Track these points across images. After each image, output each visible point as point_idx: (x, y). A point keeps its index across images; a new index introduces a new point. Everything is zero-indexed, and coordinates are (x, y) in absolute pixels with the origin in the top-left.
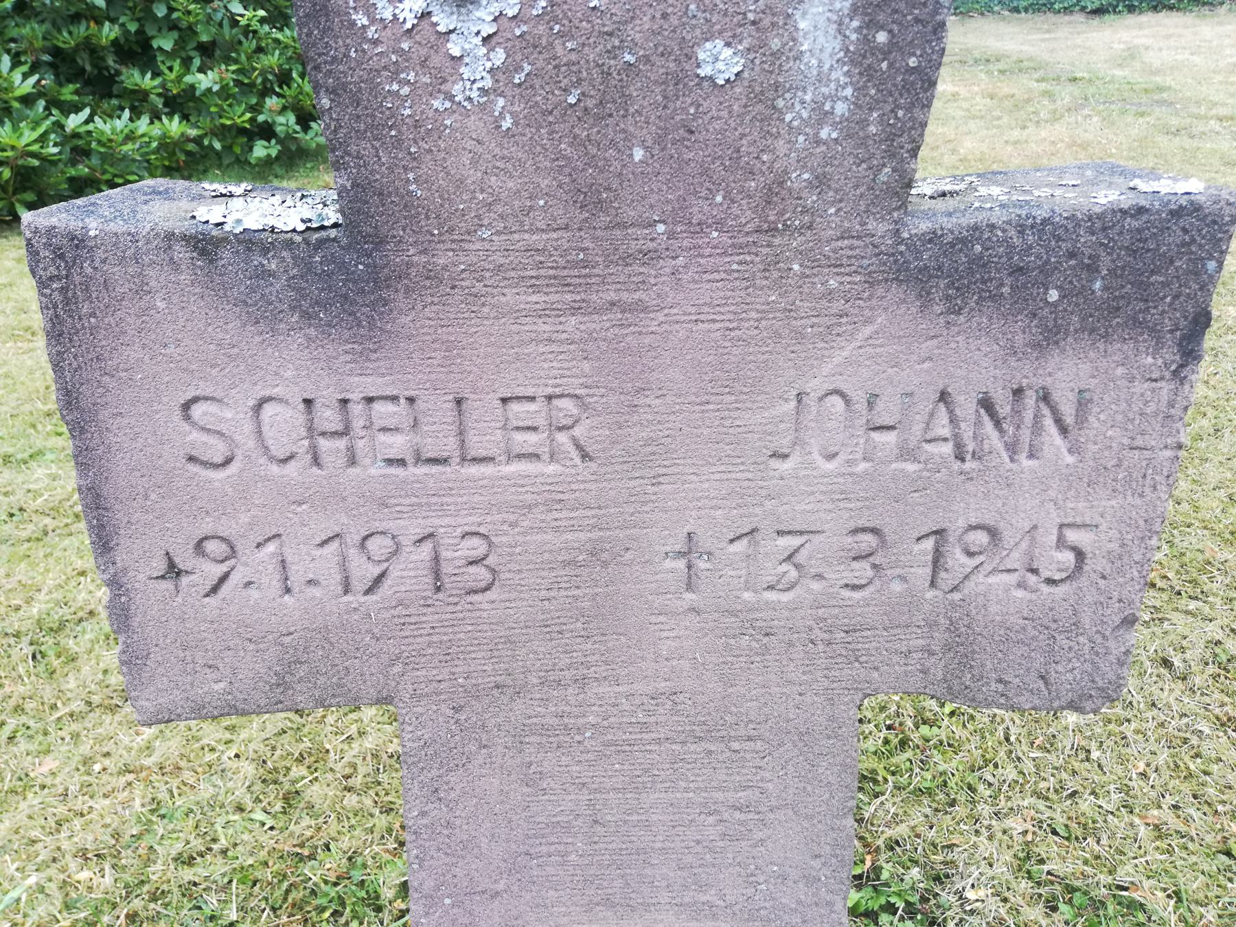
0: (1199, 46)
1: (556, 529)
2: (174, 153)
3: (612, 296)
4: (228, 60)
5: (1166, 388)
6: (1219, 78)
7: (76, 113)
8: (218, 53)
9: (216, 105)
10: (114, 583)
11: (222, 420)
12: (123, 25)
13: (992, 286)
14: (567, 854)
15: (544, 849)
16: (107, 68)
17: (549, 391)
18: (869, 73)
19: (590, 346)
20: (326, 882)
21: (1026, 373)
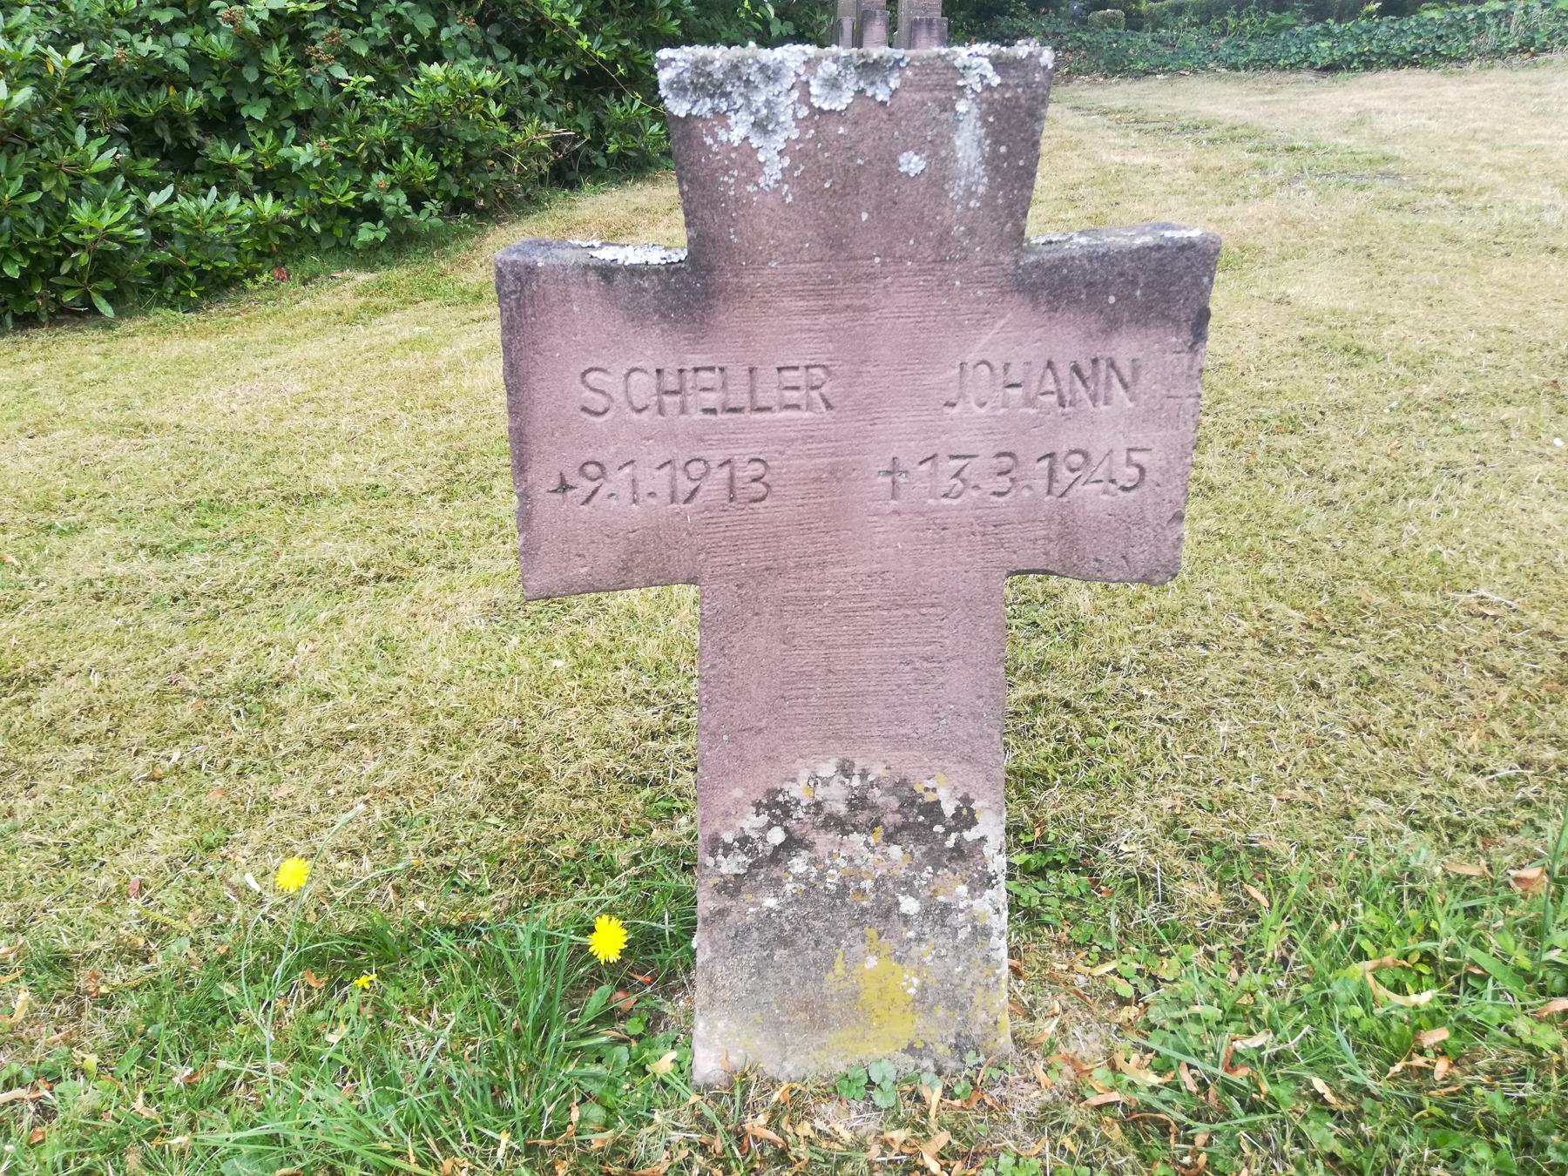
0: (1440, 110)
1: (809, 456)
2: (267, 237)
3: (847, 302)
4: (327, 131)
5: (1186, 358)
6: (1457, 146)
7: (158, 191)
8: (315, 123)
9: (316, 182)
10: (524, 496)
11: (605, 383)
12: (207, 91)
13: (1075, 294)
14: (807, 697)
15: (794, 693)
16: (189, 141)
17: (808, 363)
18: (997, 169)
19: (833, 334)
20: (567, 859)
21: (1099, 349)
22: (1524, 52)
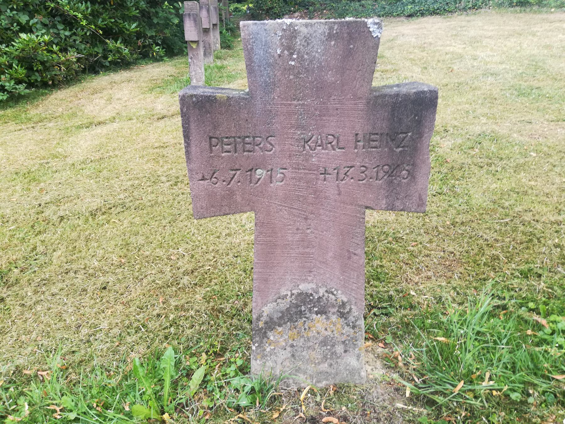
22: (474, 8)
